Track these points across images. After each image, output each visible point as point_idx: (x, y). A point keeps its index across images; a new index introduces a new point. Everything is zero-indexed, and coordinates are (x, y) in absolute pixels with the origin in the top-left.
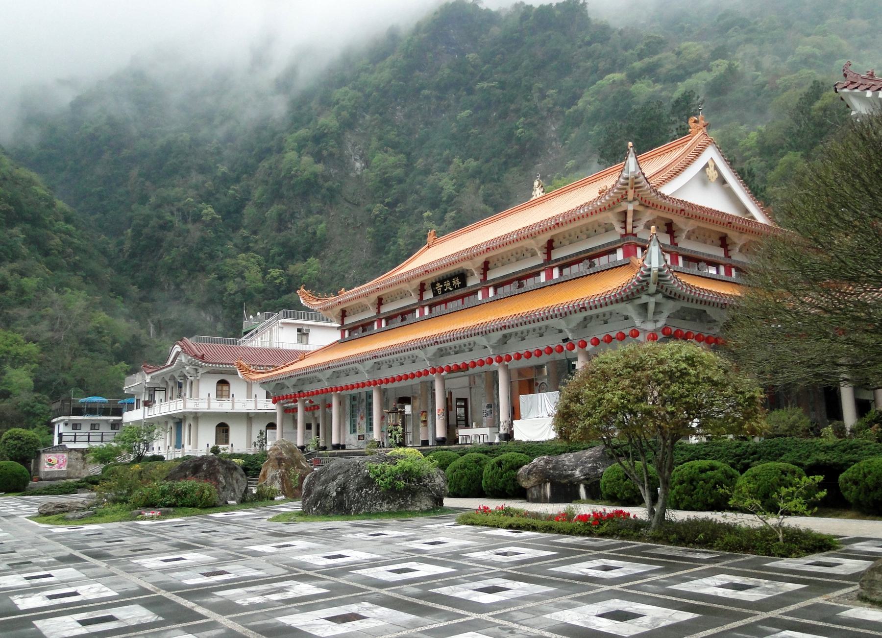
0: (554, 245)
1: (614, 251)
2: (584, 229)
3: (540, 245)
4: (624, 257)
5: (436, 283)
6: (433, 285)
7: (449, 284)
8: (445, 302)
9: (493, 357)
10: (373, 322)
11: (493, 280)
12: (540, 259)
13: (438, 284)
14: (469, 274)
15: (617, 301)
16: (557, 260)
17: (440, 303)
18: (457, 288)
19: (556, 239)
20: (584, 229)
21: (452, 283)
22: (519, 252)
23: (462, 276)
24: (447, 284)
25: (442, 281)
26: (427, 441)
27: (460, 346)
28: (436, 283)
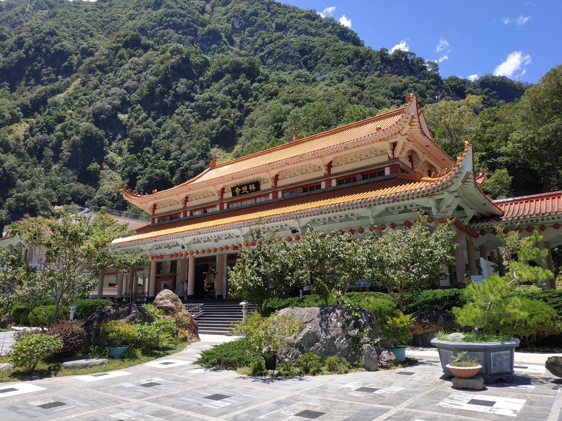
0: (279, 177)
1: (215, 206)
2: (358, 154)
3: (271, 177)
4: (337, 185)
5: (236, 187)
6: (233, 189)
7: (246, 189)
8: (241, 201)
9: (188, 252)
10: (180, 213)
11: (283, 186)
12: (217, 198)
13: (237, 189)
14: (262, 183)
15: (423, 196)
16: (226, 199)
17: (236, 201)
18: (253, 191)
19: (280, 174)
20: (358, 154)
21: (248, 188)
22: (304, 169)
23: (257, 184)
24: (245, 188)
25: (240, 187)
26: (222, 296)
27: (282, 226)
28: (236, 187)
